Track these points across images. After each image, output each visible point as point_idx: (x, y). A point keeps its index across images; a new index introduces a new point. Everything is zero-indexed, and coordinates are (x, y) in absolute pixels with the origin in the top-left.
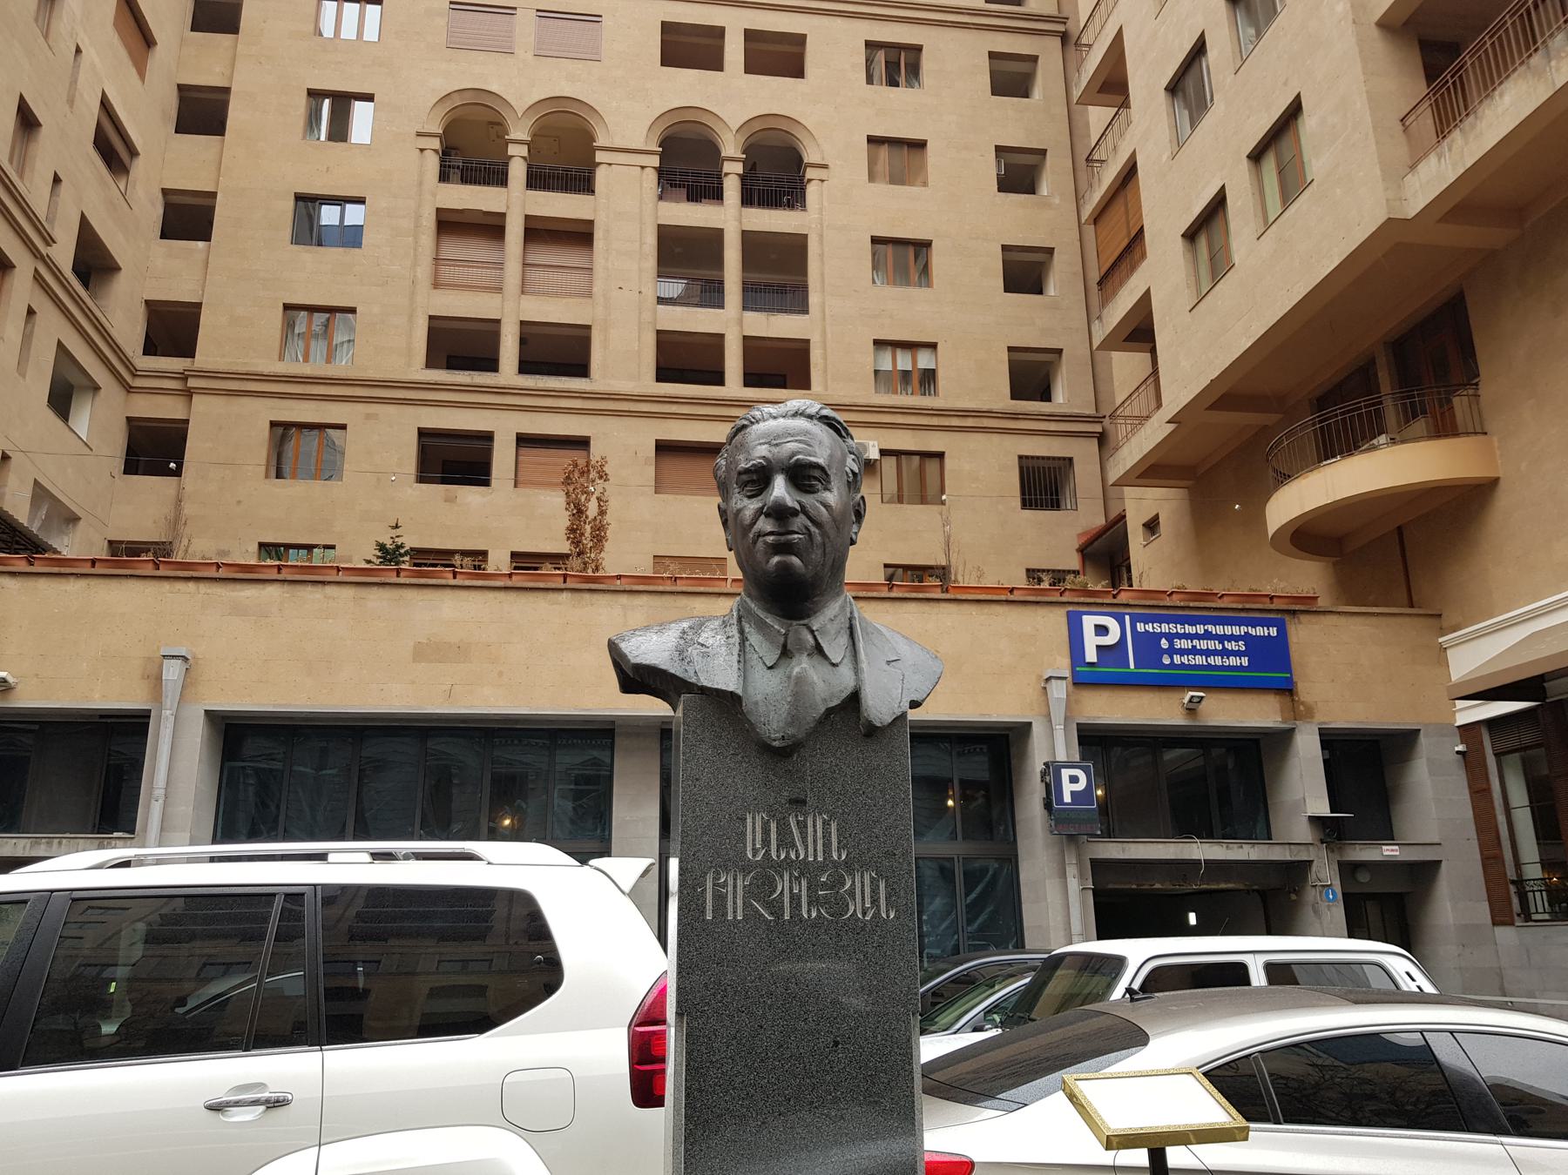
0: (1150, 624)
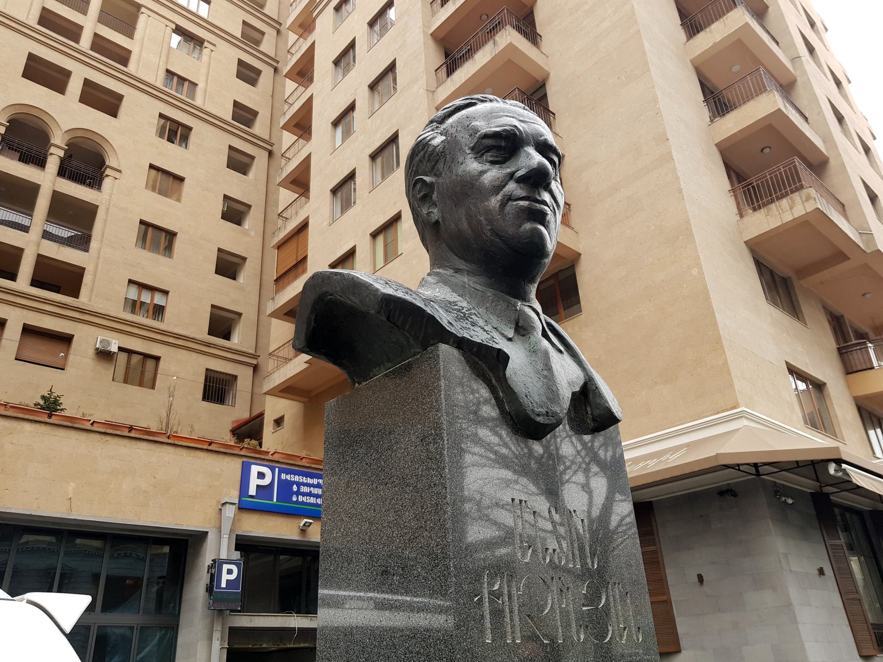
0: (289, 475)
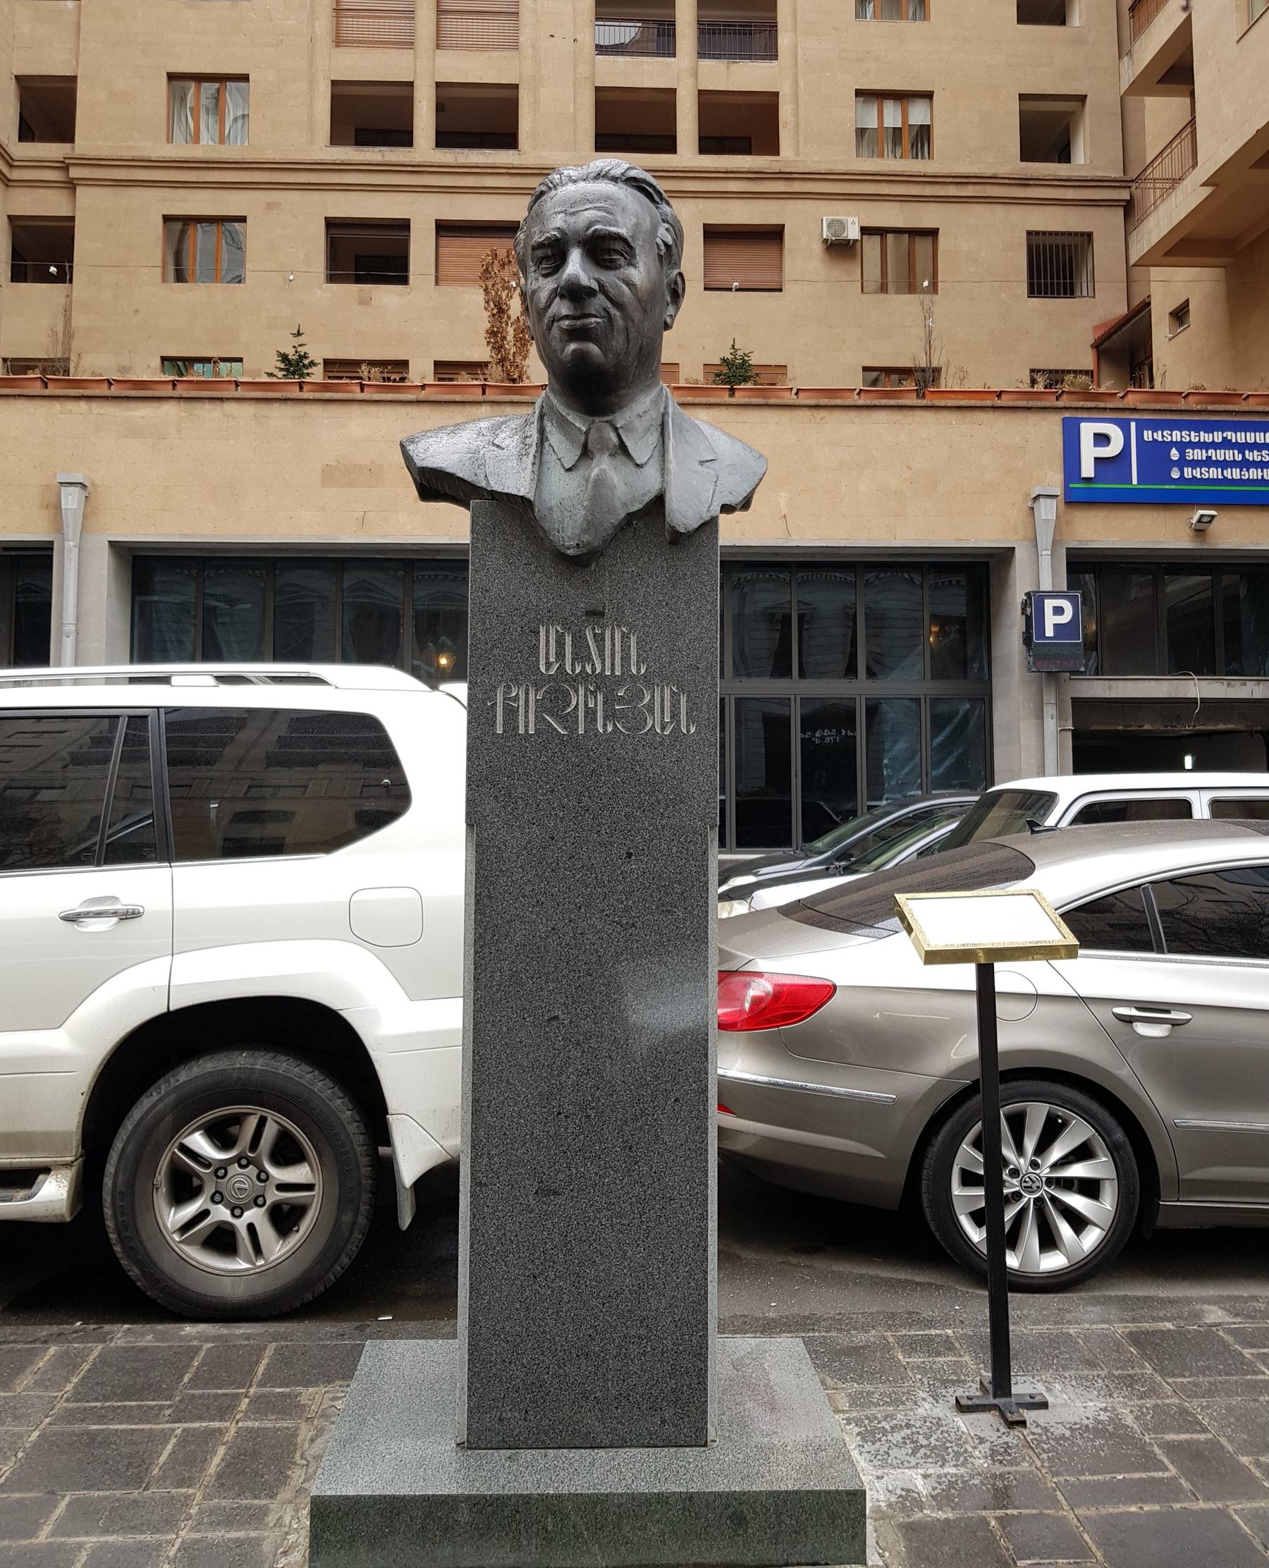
0: (1160, 432)
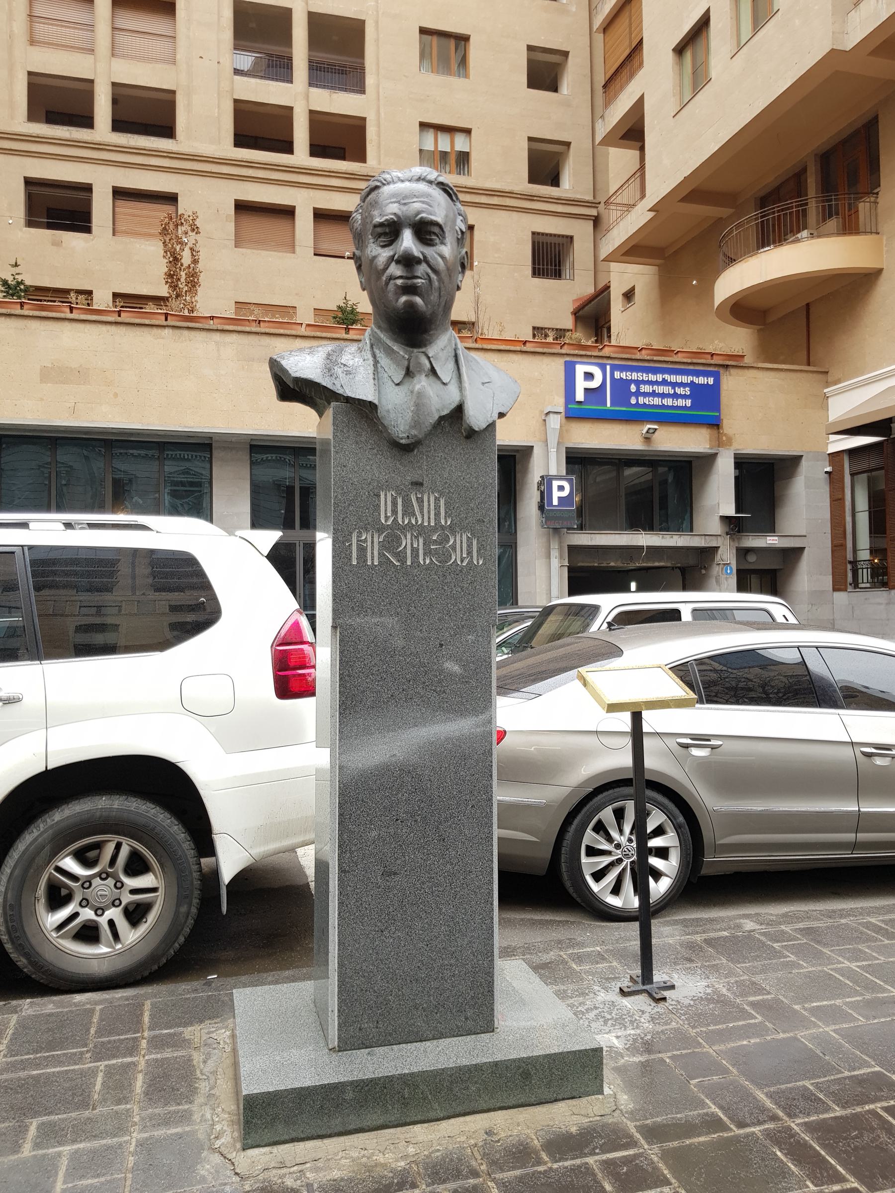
0: (624, 373)
